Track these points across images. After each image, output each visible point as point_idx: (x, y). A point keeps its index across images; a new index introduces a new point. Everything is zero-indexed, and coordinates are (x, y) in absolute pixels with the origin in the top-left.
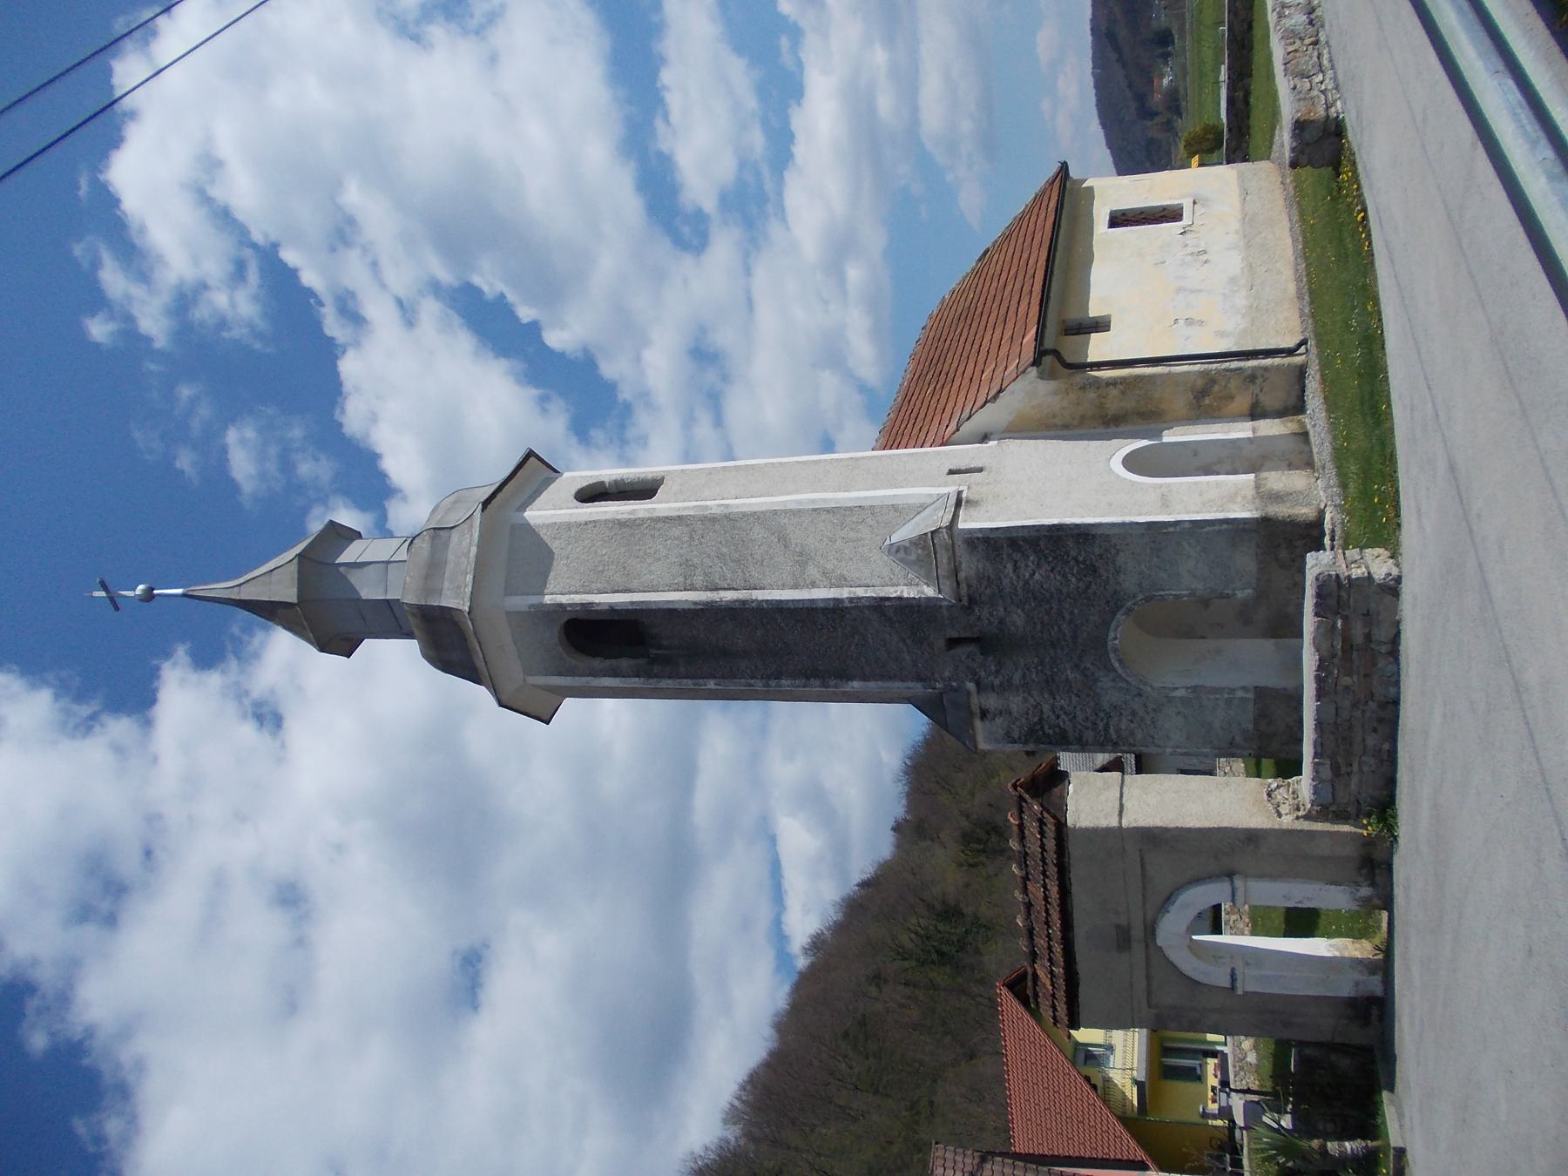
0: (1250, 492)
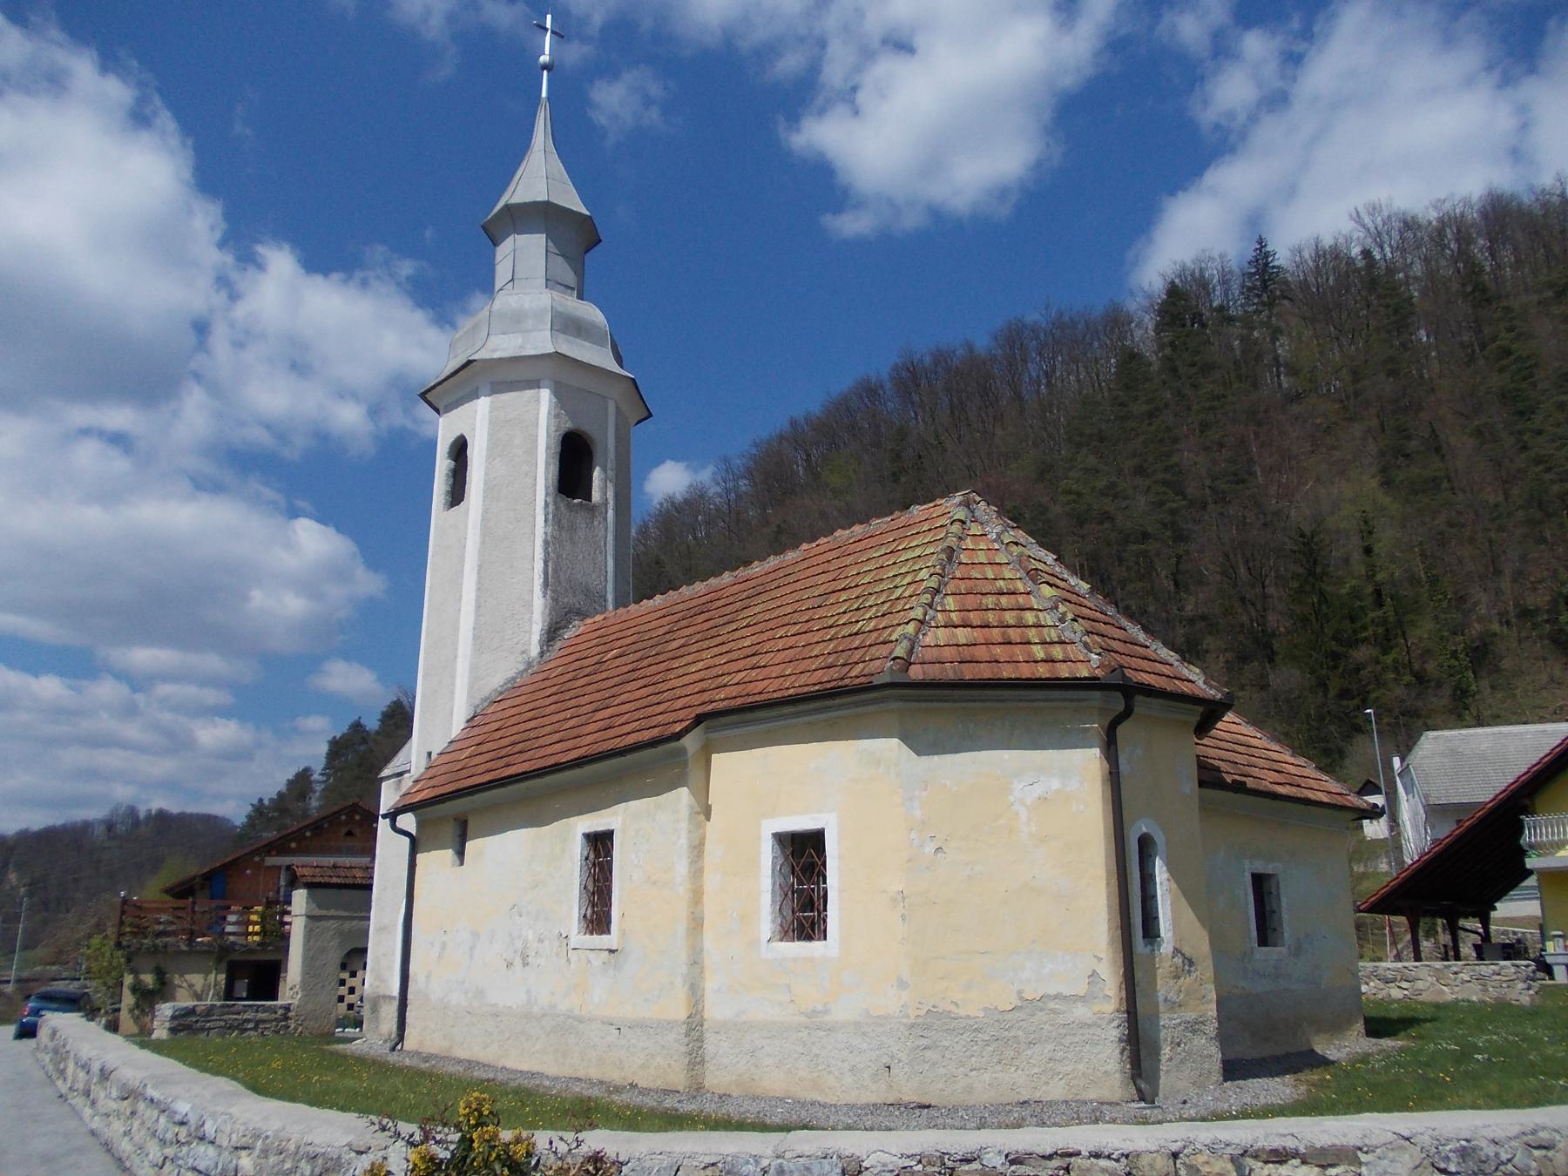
0: (382, 991)
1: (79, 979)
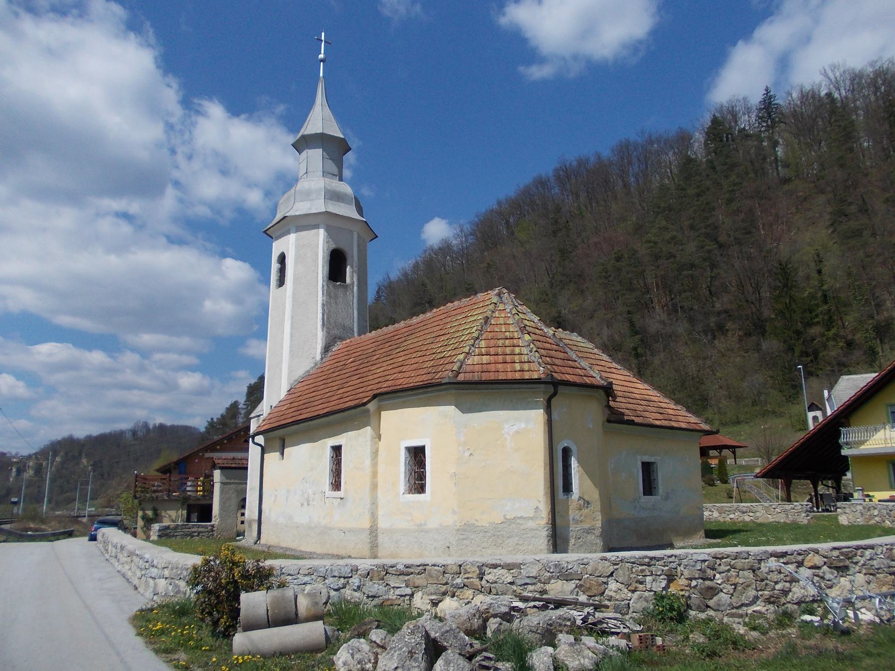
1: (121, 515)
